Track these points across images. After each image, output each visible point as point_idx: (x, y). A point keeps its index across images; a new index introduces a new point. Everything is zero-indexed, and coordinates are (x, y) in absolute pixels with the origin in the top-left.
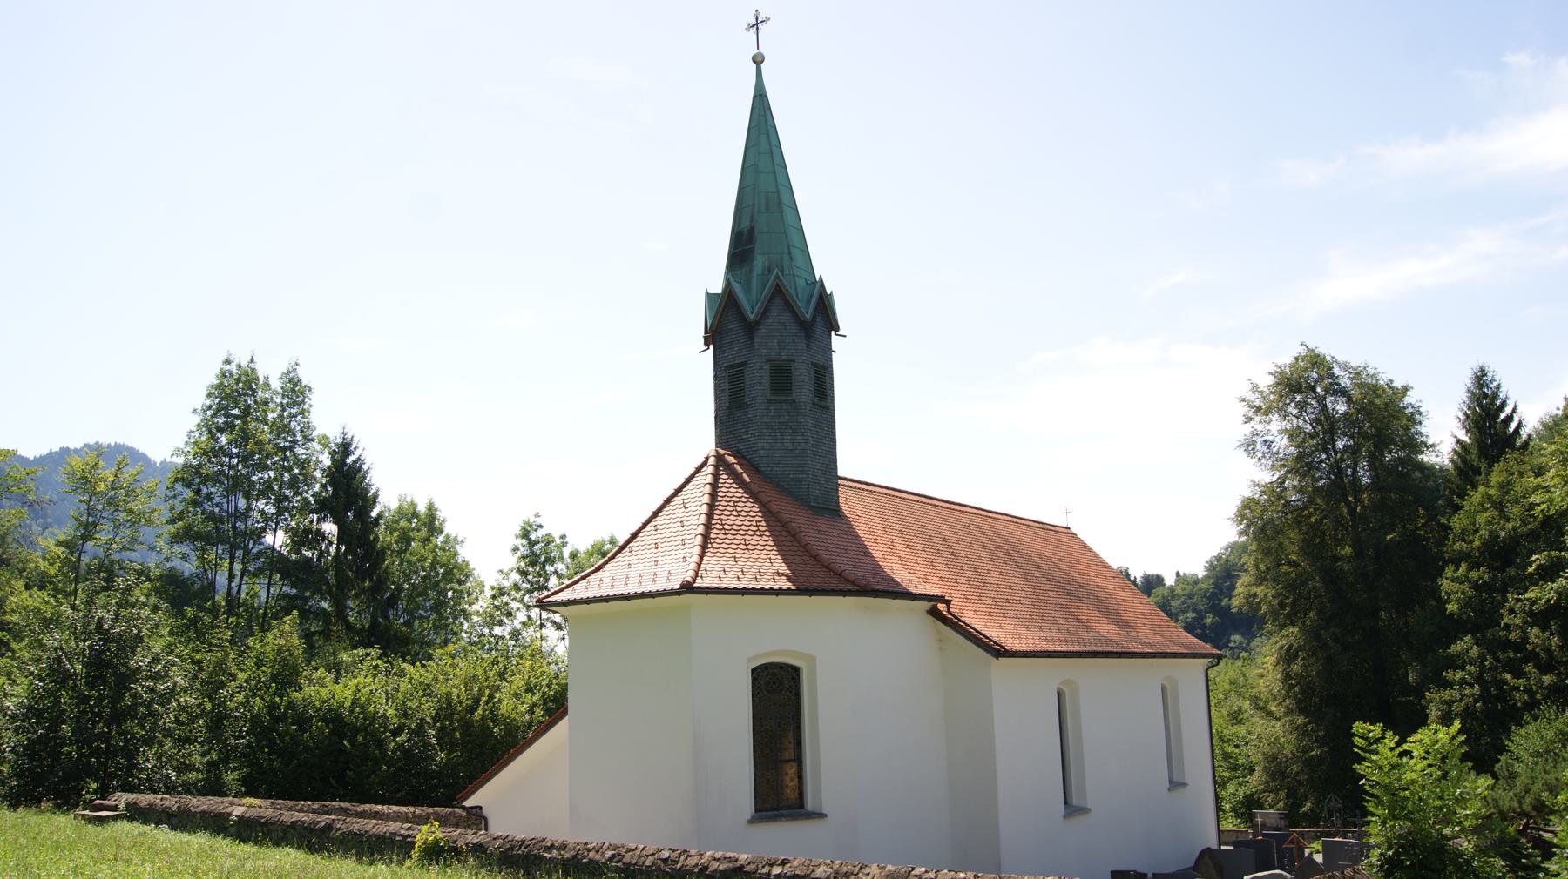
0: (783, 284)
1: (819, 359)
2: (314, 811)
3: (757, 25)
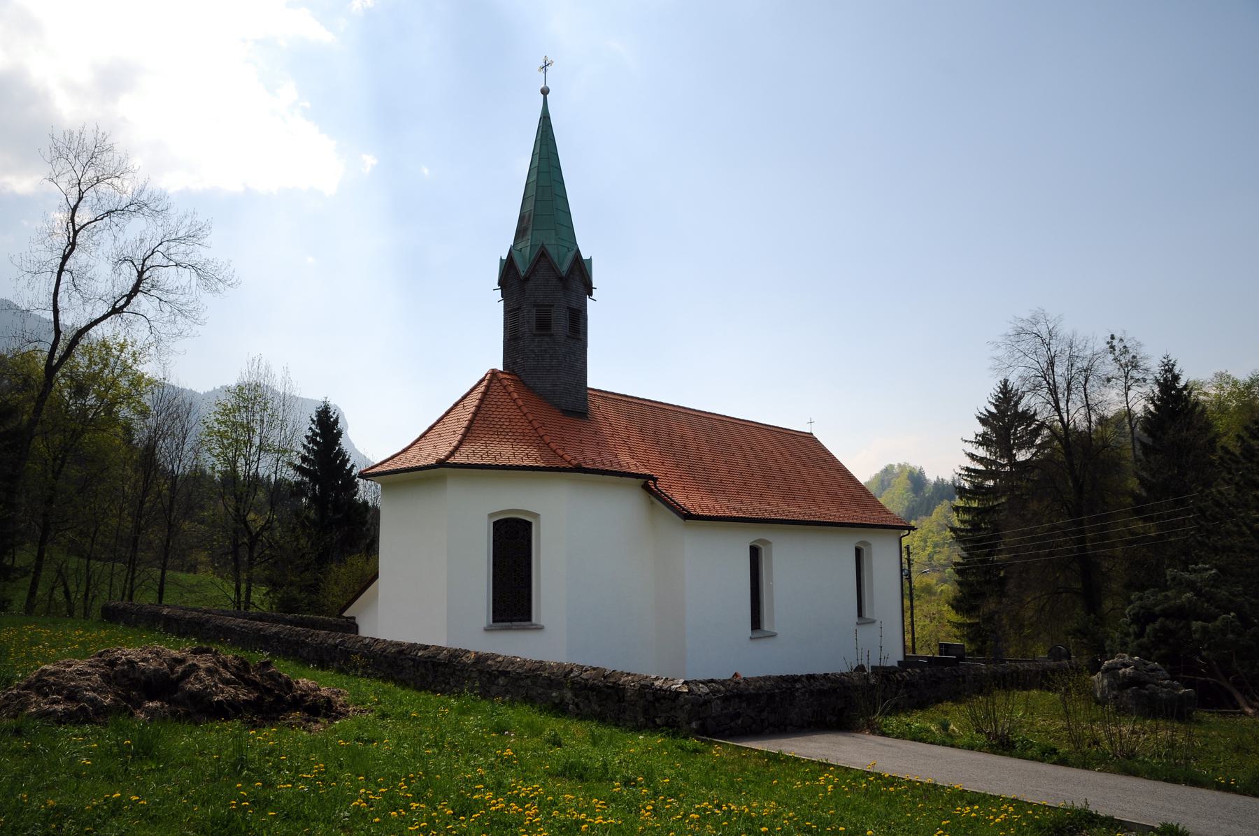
0: (547, 251)
1: (575, 306)
2: (291, 622)
3: (545, 66)
